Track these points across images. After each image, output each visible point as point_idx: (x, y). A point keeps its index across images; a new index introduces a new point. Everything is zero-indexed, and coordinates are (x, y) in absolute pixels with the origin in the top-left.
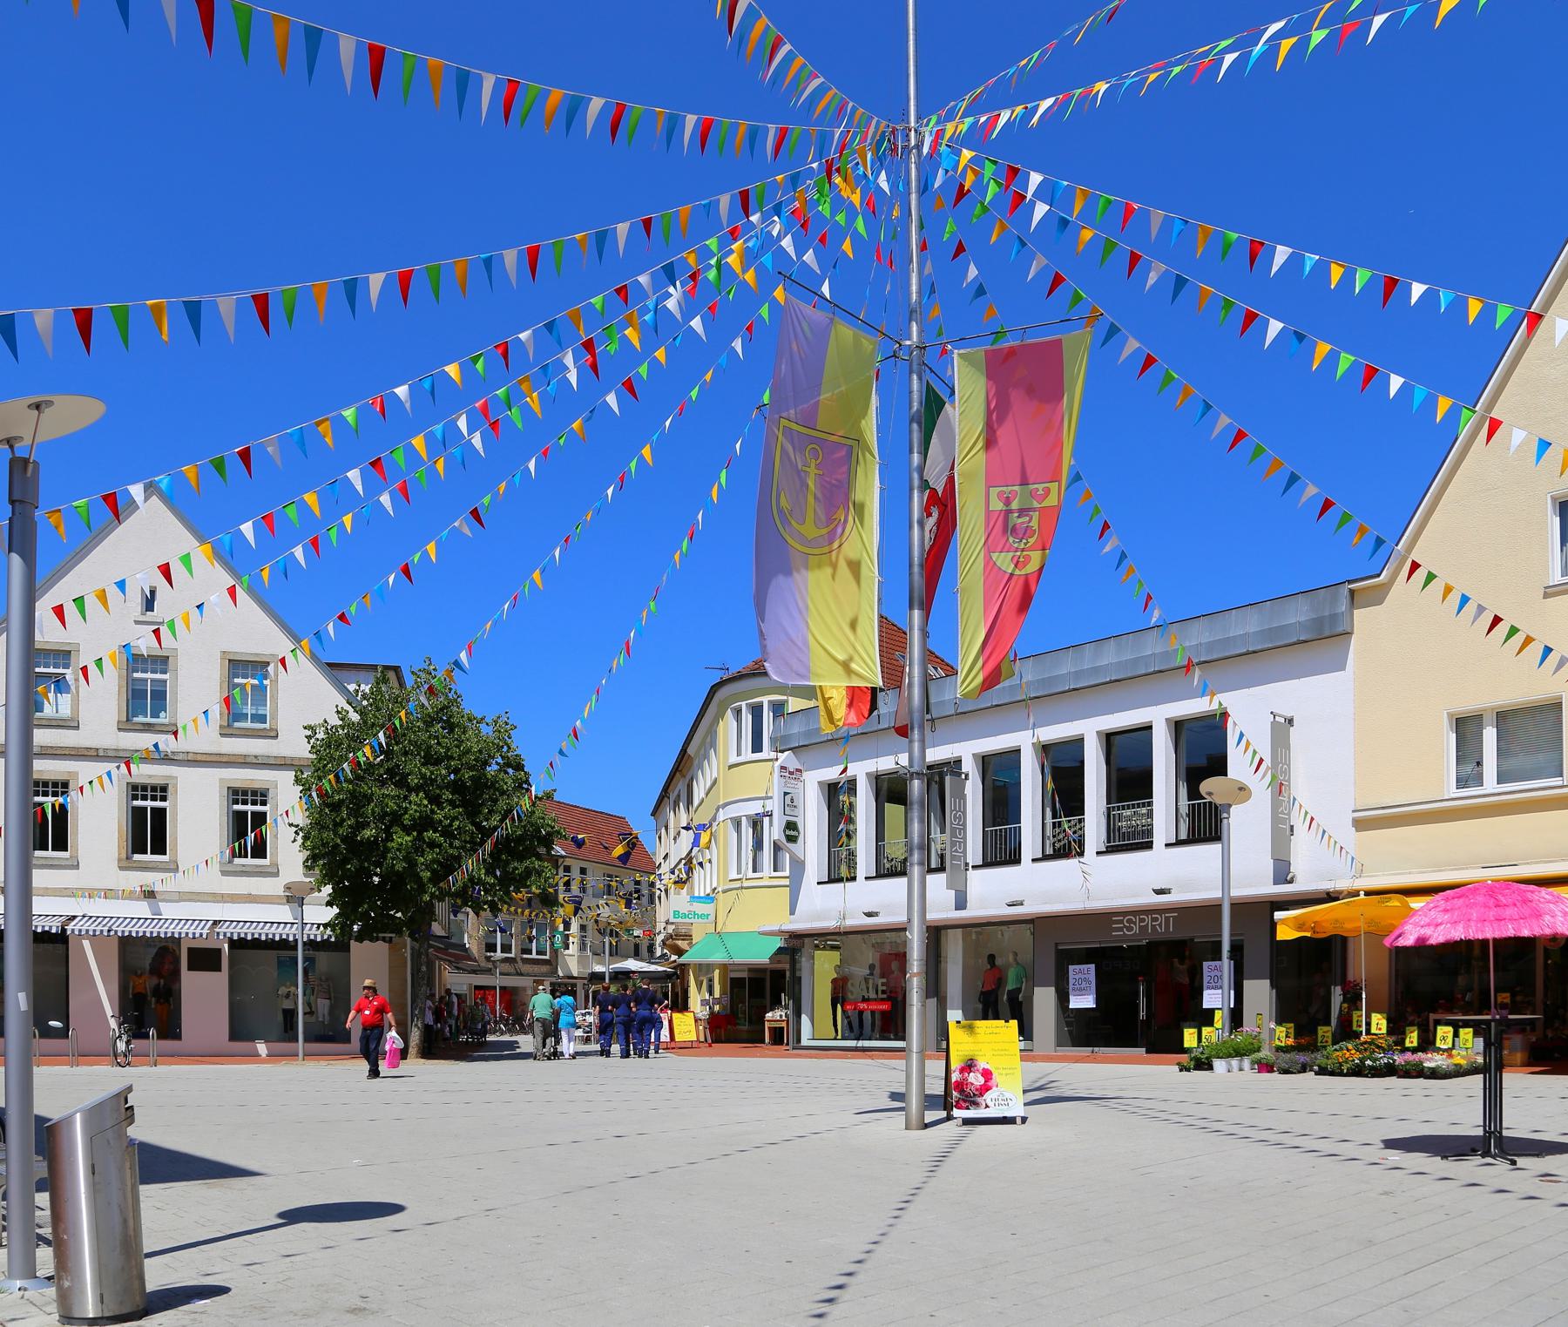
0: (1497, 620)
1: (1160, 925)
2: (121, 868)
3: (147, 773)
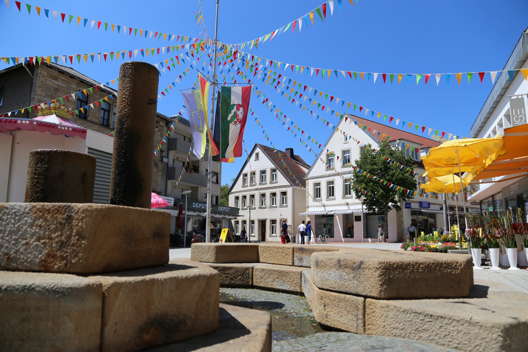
2: (343, 199)
3: (330, 179)
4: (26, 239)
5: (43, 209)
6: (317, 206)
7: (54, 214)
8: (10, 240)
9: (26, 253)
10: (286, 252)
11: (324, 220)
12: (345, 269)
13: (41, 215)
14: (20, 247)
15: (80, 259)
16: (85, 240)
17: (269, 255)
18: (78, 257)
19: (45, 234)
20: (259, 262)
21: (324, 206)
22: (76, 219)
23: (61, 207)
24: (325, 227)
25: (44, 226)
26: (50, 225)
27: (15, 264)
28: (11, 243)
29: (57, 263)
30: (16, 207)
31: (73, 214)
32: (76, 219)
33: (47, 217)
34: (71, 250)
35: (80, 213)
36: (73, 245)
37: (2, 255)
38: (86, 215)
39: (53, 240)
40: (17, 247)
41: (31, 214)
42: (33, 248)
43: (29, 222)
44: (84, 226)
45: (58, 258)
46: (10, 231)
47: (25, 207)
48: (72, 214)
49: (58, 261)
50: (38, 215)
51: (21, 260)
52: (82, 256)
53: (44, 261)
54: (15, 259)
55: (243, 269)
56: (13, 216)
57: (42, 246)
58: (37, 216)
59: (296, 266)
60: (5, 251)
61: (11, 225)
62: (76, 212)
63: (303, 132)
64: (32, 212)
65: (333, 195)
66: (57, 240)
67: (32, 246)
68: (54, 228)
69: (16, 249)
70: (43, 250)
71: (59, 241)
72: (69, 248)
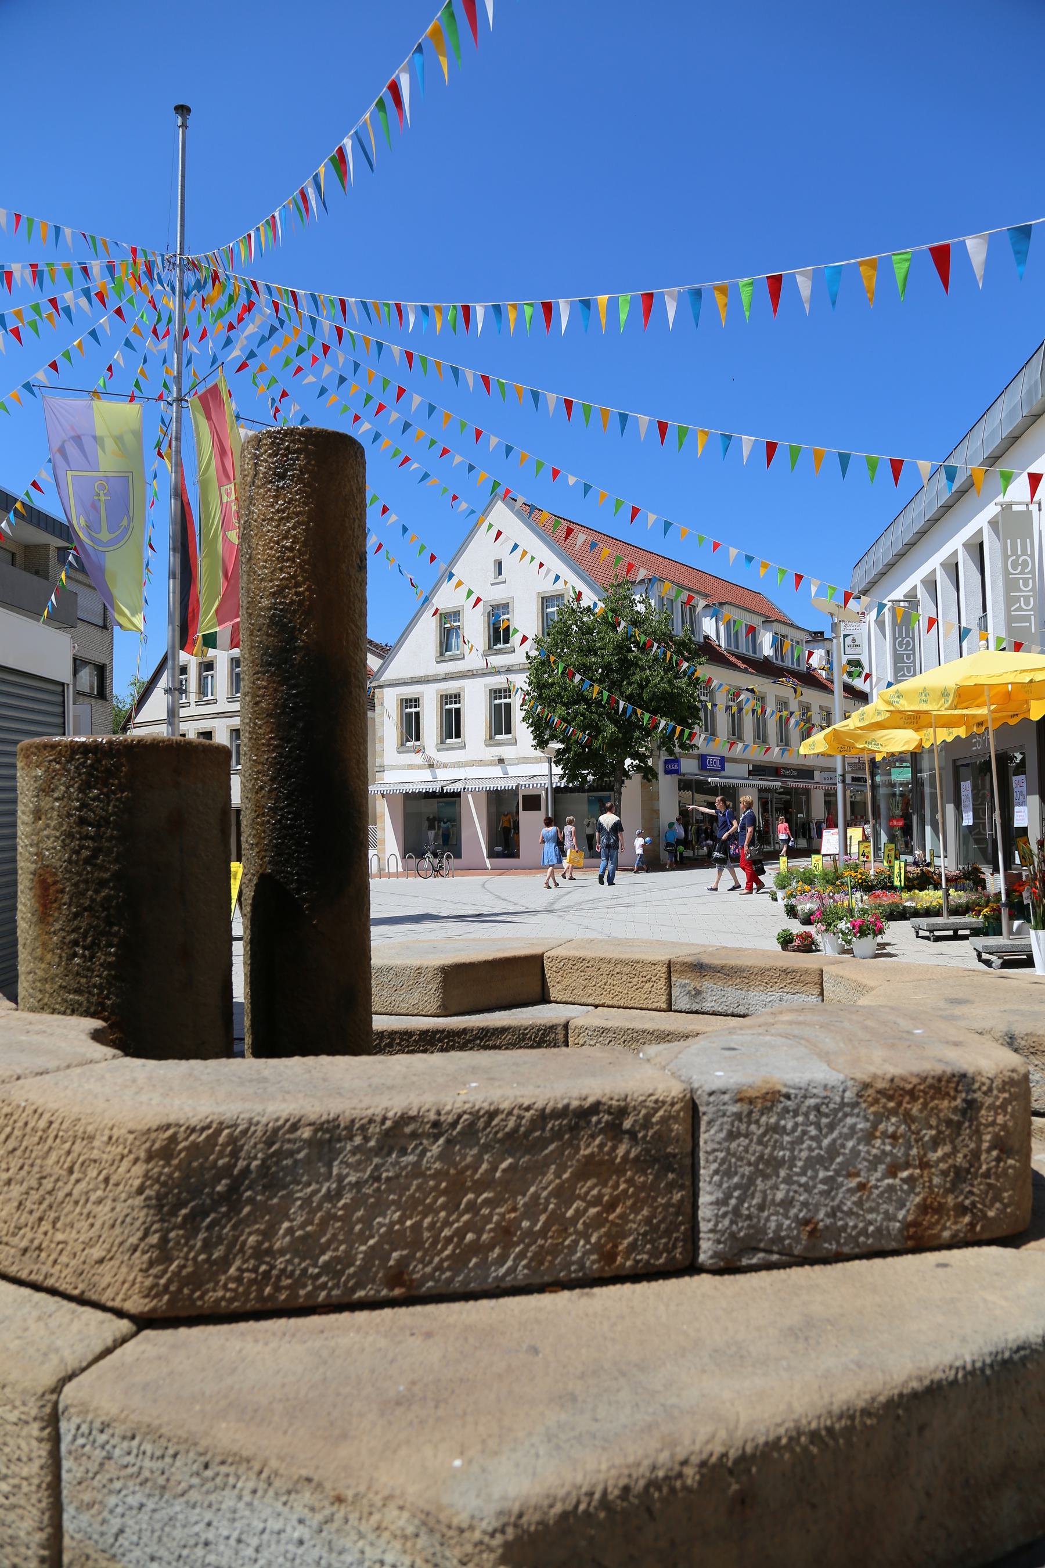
0: (516, 546)
1: (1020, 609)
2: (487, 746)
3: (451, 687)
4: (857, 1175)
5: (895, 1091)
6: (411, 767)
7: (929, 1099)
8: (811, 1183)
9: (861, 1212)
10: (645, 974)
11: (431, 808)
12: (1032, 1057)
13: (892, 1108)
14: (844, 1197)
15: (1006, 1206)
16: (1013, 1159)
17: (584, 983)
18: (1001, 1201)
19: (908, 1155)
20: (550, 1002)
21: (431, 766)
22: (989, 1108)
23: (945, 1079)
24: (431, 827)
25: (903, 1136)
26: (921, 1130)
27: (831, 1244)
28: (816, 1191)
29: (948, 1224)
30: (815, 1091)
31: (978, 1095)
32: (989, 1108)
33: (911, 1109)
34: (982, 1187)
35: (995, 1092)
36: (987, 1175)
37: (793, 1225)
38: (1010, 1094)
39: (932, 1166)
40: (833, 1199)
41: (864, 1105)
42: (880, 1196)
43: (861, 1130)
44: (1010, 1124)
45: (949, 1210)
46: (808, 1159)
47: (841, 1089)
48: (975, 1095)
49: (949, 1219)
50: (884, 1107)
51: (849, 1230)
52: (1010, 1197)
53: (915, 1224)
54: (833, 1232)
55: (539, 1030)
56: (812, 1117)
57: (905, 1187)
58: (881, 1110)
59: (681, 1012)
60: (801, 1215)
61: (808, 1142)
62: (984, 1088)
63: (433, 558)
64: (865, 1101)
65: (458, 736)
66: (943, 1166)
67: (876, 1192)
68: (932, 1138)
69: (831, 1204)
70: (909, 1196)
71: (950, 1167)
72: (976, 1183)
